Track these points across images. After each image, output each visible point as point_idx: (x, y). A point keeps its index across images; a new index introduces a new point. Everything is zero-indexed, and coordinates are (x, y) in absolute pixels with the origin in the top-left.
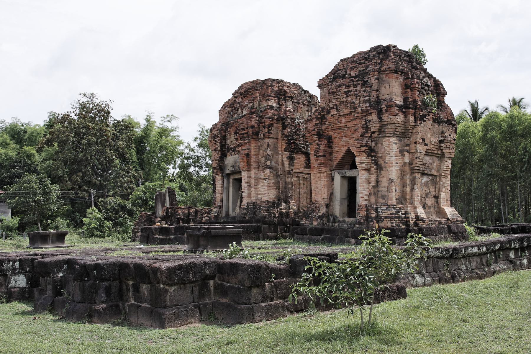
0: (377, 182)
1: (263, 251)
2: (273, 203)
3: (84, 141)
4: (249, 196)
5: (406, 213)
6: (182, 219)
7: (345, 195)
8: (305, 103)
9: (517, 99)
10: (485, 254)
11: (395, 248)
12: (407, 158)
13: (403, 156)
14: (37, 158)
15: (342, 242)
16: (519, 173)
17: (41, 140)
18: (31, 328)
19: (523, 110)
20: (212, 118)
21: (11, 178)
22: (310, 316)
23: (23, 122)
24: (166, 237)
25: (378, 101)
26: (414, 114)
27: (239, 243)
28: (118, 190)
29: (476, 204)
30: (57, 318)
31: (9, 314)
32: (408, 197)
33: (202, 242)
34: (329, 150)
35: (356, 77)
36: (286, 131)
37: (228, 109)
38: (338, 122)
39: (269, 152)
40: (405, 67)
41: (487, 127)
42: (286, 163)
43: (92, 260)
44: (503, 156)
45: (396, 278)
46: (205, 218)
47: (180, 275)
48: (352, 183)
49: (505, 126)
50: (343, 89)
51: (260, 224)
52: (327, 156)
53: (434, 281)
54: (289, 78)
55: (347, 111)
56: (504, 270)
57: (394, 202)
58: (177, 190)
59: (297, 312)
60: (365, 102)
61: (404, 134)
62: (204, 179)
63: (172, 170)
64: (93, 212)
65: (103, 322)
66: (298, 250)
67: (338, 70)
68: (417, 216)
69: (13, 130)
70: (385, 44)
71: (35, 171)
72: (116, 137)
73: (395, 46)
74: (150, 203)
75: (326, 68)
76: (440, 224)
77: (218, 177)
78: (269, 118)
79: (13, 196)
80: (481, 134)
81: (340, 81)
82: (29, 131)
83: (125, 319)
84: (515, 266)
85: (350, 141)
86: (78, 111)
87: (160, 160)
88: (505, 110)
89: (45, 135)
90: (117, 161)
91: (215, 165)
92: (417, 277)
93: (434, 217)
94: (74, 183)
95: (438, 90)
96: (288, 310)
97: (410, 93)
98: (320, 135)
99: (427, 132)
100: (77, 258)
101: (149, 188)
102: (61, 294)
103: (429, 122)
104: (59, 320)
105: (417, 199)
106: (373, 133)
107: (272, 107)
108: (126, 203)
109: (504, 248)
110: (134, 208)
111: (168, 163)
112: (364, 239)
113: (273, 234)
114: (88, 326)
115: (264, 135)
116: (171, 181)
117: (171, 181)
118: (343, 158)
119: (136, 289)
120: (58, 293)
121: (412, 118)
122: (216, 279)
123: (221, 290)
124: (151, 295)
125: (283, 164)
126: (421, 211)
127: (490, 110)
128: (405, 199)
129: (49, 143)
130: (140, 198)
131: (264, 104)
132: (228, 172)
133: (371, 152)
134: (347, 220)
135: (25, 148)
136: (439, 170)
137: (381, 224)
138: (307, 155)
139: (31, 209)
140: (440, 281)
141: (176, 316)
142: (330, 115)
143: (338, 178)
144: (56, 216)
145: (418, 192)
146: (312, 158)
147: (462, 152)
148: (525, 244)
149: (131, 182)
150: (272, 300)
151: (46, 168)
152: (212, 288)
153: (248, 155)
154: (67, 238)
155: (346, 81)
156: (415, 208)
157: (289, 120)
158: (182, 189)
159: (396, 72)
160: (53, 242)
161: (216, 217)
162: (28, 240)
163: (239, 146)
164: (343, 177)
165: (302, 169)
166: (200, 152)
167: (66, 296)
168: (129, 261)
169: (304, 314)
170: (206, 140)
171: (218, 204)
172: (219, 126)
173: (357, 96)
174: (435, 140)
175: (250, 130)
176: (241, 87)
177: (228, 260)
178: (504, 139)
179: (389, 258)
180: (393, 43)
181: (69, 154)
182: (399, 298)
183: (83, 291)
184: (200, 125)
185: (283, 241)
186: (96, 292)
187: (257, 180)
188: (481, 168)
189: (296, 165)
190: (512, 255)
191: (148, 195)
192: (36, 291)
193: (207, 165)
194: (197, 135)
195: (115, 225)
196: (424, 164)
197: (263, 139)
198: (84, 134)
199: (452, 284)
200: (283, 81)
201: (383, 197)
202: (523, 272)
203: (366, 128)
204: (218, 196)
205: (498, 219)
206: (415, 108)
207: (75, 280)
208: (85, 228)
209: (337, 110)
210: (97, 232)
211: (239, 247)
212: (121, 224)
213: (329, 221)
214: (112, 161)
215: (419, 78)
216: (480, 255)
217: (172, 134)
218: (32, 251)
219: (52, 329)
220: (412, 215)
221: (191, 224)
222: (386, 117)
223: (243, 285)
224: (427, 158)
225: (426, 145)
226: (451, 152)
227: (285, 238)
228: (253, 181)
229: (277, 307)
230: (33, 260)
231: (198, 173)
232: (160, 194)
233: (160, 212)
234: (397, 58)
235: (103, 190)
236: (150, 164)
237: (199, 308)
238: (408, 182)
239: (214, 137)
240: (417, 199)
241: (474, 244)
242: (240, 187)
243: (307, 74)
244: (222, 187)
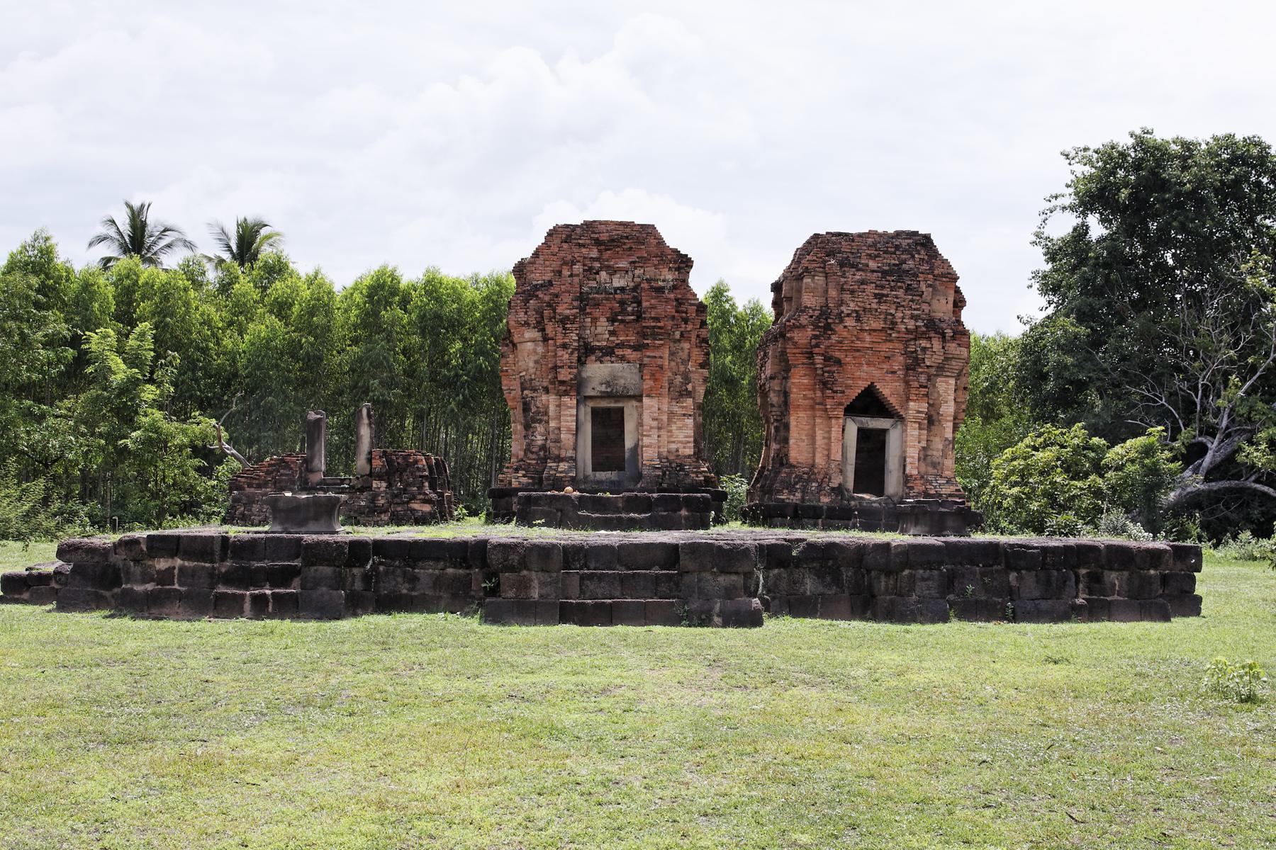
38: (858, 339)
115: (682, 335)
142: (841, 326)
173: (898, 305)
197: (679, 341)
201: (934, 465)
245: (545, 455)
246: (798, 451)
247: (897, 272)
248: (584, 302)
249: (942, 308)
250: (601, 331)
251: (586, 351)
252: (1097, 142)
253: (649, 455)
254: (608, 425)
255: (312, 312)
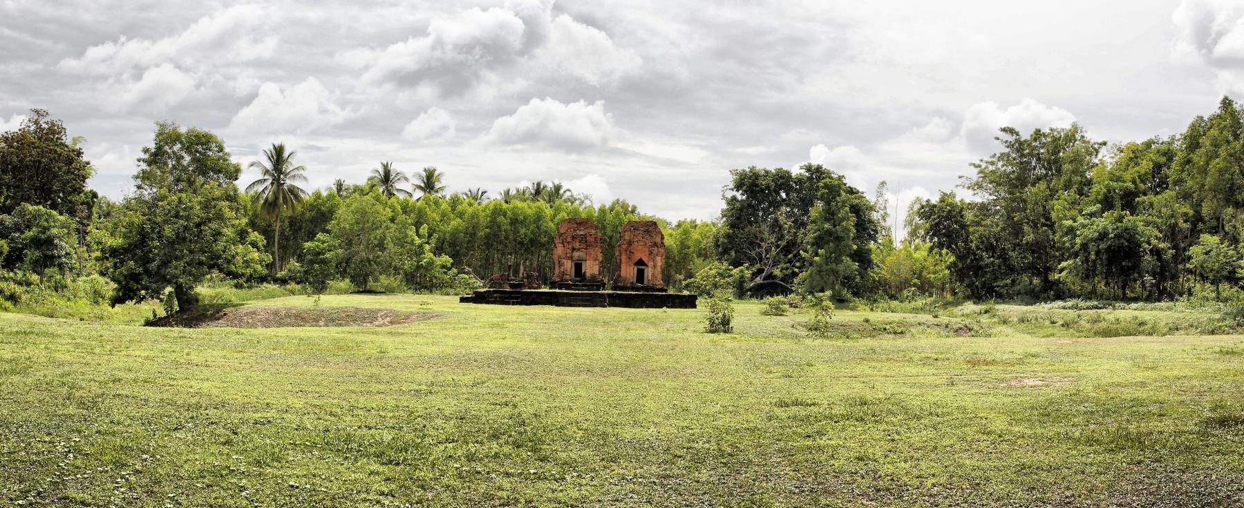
245: (564, 274)
246: (623, 273)
247: (647, 231)
248: (573, 238)
249: (658, 240)
250: (577, 245)
251: (574, 249)
252: (740, 169)
253: (588, 275)
254: (578, 267)
255: (473, 217)
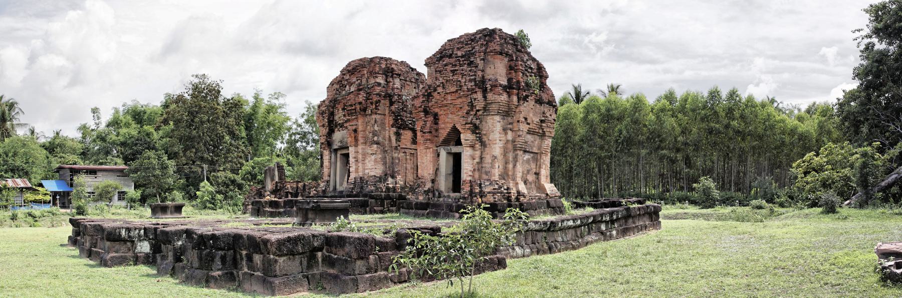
0: (481, 158)
1: (369, 224)
2: (380, 178)
3: (197, 120)
4: (357, 170)
5: (508, 189)
6: (291, 193)
7: (450, 170)
8: (413, 80)
9: (615, 86)
10: (580, 226)
11: (495, 222)
12: (510, 136)
13: (506, 134)
14: (156, 136)
15: (446, 216)
16: (614, 153)
17: (159, 119)
18: (156, 289)
19: (619, 96)
20: (319, 95)
21: (134, 155)
22: (413, 286)
23: (142, 103)
24: (275, 209)
25: (483, 81)
26: (518, 94)
27: (346, 217)
28: (228, 165)
29: (576, 181)
30: (178, 281)
31: (137, 276)
32: (510, 173)
33: (310, 216)
34: (435, 127)
35: (462, 56)
36: (393, 108)
37: (336, 86)
39: (376, 128)
40: (510, 49)
41: (588, 110)
42: (393, 138)
43: (207, 230)
44: (601, 137)
45: (496, 250)
46: (313, 192)
47: (289, 247)
48: (457, 159)
49: (603, 110)
50: (449, 68)
51: (364, 200)
52: (434, 132)
53: (532, 253)
54: (397, 56)
55: (453, 89)
56: (596, 241)
57: (496, 178)
58: (285, 165)
59: (400, 282)
60: (470, 81)
61: (507, 113)
62: (311, 154)
63: (280, 145)
64: (205, 185)
65: (220, 287)
66: (403, 224)
67: (445, 50)
68: (518, 192)
69: (134, 111)
70: (491, 28)
71: (154, 148)
72: (226, 115)
73: (500, 30)
74: (259, 177)
75: (433, 48)
76: (539, 199)
77: (326, 153)
78: (377, 94)
79: (136, 171)
80: (582, 115)
81: (447, 60)
82: (148, 112)
83: (239, 286)
84: (605, 236)
85: (456, 118)
86: (191, 92)
87: (268, 136)
88: (604, 94)
89: (162, 115)
90: (227, 138)
91: (323, 140)
92: (517, 248)
93: (535, 193)
94: (188, 158)
95: (541, 72)
96: (392, 281)
97: (514, 74)
98: (426, 112)
99: (529, 111)
100: (194, 228)
101: (258, 163)
102: (181, 261)
103: (531, 102)
104: (180, 283)
105: (519, 175)
106: (478, 111)
107: (379, 84)
108: (236, 177)
109: (596, 221)
110: (243, 182)
111: (275, 139)
112: (466, 213)
113: (380, 208)
114: (206, 290)
116: (278, 156)
117: (278, 156)
118: (449, 134)
119: (250, 259)
120: (178, 259)
121: (515, 98)
122: (324, 251)
123: (330, 262)
124: (263, 264)
125: (390, 140)
126: (522, 188)
127: (591, 93)
128: (508, 175)
129: (165, 122)
130: (250, 173)
131: (372, 81)
132: (335, 147)
133: (475, 129)
134: (452, 195)
135: (145, 127)
136: (540, 148)
137: (484, 199)
138: (414, 131)
139: (150, 183)
140: (538, 253)
141: (285, 285)
143: (443, 154)
144: (173, 189)
145: (520, 168)
146: (419, 134)
147: (565, 132)
148: (615, 217)
149: (241, 157)
150: (376, 272)
151: (163, 145)
152: (320, 260)
153: (355, 131)
154: (184, 209)
155: (452, 60)
156: (517, 184)
157: (396, 97)
158: (290, 164)
159: (501, 54)
160: (171, 213)
161: (324, 191)
162: (149, 210)
163: (346, 122)
164: (449, 153)
165: (409, 145)
166: (307, 128)
167: (185, 262)
168: (242, 232)
169: (407, 284)
170: (313, 116)
171: (326, 178)
172: (327, 103)
173: (463, 75)
174: (536, 120)
175: (358, 107)
176: (349, 64)
177: (335, 233)
178: (602, 121)
179: (488, 231)
180: (498, 27)
181: (183, 131)
182: (499, 269)
183: (200, 259)
184: (306, 102)
185: (389, 215)
186: (213, 261)
187: (365, 155)
188: (582, 147)
189: (403, 141)
190: (603, 227)
191: (257, 170)
192: (158, 257)
193: (314, 141)
194: (304, 111)
195: (226, 198)
196: (526, 142)
198: (197, 113)
199: (549, 255)
200: (390, 59)
201: (487, 173)
202: (611, 242)
203: (472, 106)
204: (326, 171)
205: (595, 195)
206: (519, 89)
207: (193, 248)
208: (199, 200)
209: (444, 88)
210: (211, 204)
211: (346, 221)
212: (232, 198)
213: (434, 196)
214: (223, 137)
215: (523, 61)
216: (575, 227)
217: (279, 111)
218: (154, 221)
219: (174, 291)
220: (514, 191)
221: (299, 198)
222: (490, 96)
223: (350, 257)
224: (529, 136)
225: (528, 124)
226: (552, 131)
227: (391, 212)
228: (360, 156)
229: (380, 279)
230: (156, 229)
231: (305, 148)
232: (270, 168)
233: (270, 186)
234: (503, 41)
235: (215, 165)
236: (258, 140)
237: (307, 278)
238: (511, 159)
239: (322, 113)
240: (519, 175)
241: (570, 218)
242: (348, 162)
243: (415, 52)
244: (330, 162)
